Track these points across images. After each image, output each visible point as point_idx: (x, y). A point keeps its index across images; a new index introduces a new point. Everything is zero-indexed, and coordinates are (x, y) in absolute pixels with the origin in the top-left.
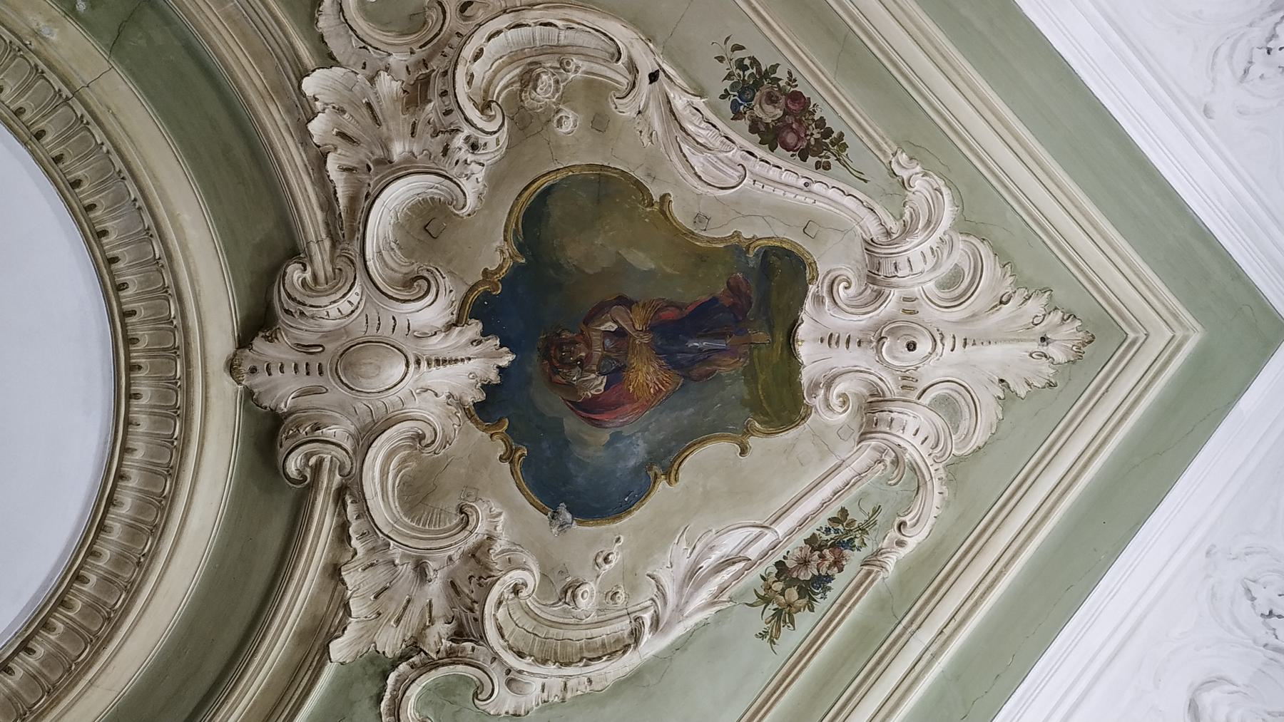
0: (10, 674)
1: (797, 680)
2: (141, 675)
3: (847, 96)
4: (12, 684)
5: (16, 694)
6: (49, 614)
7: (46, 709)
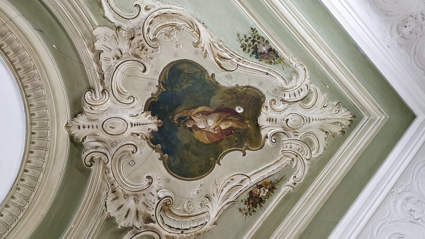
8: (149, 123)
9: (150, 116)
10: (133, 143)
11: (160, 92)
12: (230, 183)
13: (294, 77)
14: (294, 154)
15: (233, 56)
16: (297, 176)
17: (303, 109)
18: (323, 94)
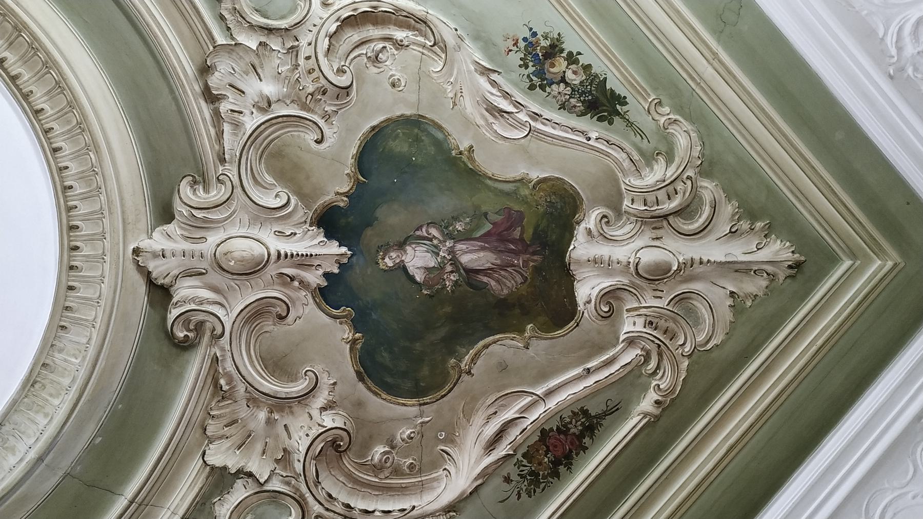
0: (6, 59)
1: (318, 54)
2: (59, 10)
3: (761, 432)
4: (14, 60)
5: (22, 57)
6: (20, 90)
7: (30, 33)
8: (318, 253)
9: (321, 238)
10: (287, 301)
11: (351, 191)
12: (497, 414)
13: (661, 160)
14: (653, 341)
15: (522, 107)
16: (662, 384)
17: (678, 234)
18: (730, 202)
